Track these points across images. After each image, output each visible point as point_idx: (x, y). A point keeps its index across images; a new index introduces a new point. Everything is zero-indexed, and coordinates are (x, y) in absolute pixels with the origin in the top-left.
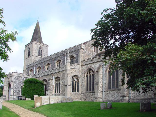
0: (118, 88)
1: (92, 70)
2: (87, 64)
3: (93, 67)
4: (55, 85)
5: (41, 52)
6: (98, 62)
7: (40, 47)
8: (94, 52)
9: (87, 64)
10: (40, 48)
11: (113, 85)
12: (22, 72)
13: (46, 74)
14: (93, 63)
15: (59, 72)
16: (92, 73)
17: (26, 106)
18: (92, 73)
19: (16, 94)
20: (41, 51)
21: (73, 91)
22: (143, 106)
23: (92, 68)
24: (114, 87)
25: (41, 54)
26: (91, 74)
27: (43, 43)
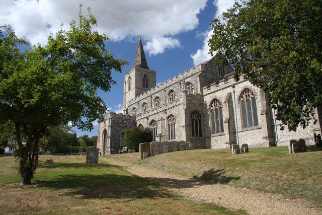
0: (258, 125)
1: (218, 101)
2: (211, 93)
3: (219, 96)
4: (167, 127)
5: (147, 82)
6: (225, 88)
8: (219, 74)
9: (211, 93)
10: (145, 76)
11: (172, 137)
12: (92, 123)
13: (155, 112)
14: (220, 90)
15: (172, 108)
16: (251, 95)
17: (180, 159)
18: (251, 95)
19: (114, 145)
20: (147, 80)
21: (193, 135)
22: (62, 177)
23: (218, 99)
24: (247, 125)
26: (249, 97)
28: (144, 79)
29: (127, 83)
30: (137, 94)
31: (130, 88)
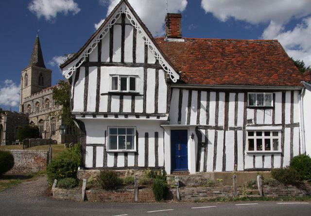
7: (41, 73)
10: (41, 75)
20: (43, 78)
25: (43, 83)
27: (45, 67)
28: (40, 78)
29: (24, 79)
30: (33, 92)
31: (26, 85)
